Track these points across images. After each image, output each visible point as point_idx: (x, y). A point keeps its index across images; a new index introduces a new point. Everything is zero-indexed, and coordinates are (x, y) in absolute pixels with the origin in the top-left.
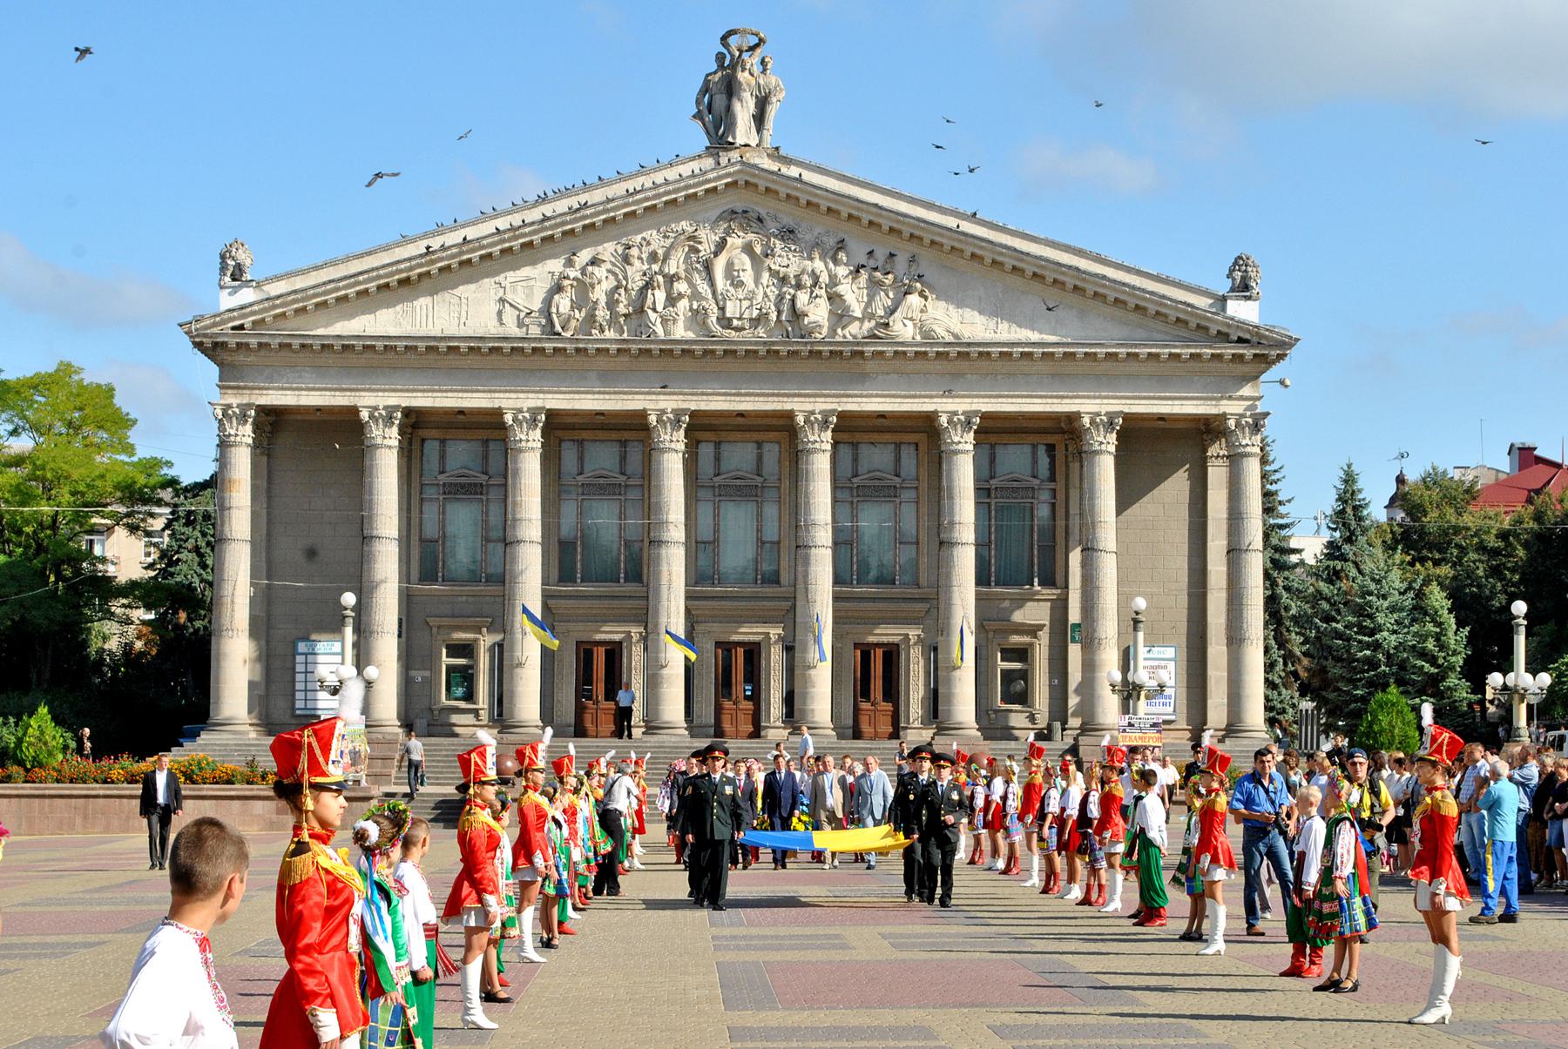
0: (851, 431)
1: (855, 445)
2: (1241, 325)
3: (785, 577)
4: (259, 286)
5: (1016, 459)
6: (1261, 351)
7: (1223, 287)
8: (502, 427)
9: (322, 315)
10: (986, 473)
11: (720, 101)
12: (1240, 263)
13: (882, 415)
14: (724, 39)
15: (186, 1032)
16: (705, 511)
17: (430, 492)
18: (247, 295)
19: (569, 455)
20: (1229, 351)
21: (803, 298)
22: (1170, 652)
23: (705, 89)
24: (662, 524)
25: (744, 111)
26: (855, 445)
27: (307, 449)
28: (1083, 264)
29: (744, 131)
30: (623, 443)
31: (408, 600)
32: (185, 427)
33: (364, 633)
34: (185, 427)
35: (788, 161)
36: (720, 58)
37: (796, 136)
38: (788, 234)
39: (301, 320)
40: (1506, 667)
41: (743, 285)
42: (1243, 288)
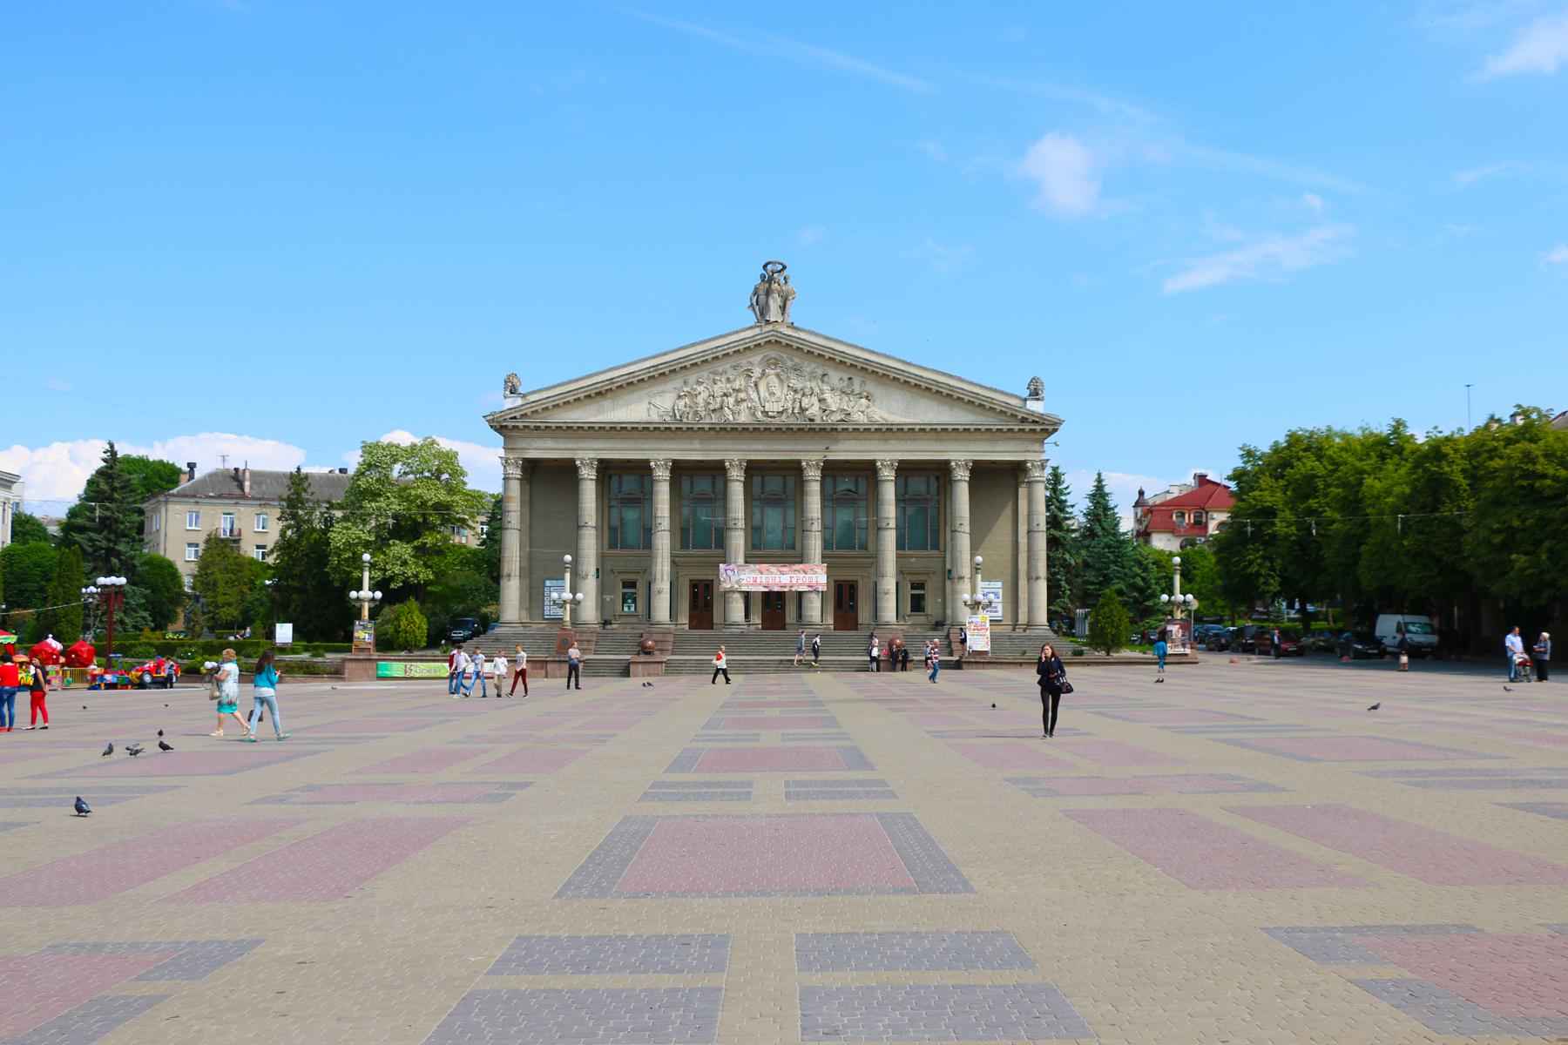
1: (834, 477)
2: (1032, 413)
3: (798, 546)
4: (524, 396)
5: (918, 485)
6: (1044, 428)
7: (1026, 394)
8: (650, 470)
9: (557, 411)
10: (902, 491)
11: (762, 298)
12: (1034, 380)
13: (847, 462)
14: (765, 267)
15: (137, 752)
16: (757, 511)
17: (614, 503)
18: (519, 402)
19: (685, 482)
20: (1027, 427)
21: (805, 401)
22: (999, 584)
23: (756, 293)
24: (732, 515)
25: (774, 304)
26: (834, 477)
27: (546, 480)
28: (952, 382)
29: (774, 314)
30: (714, 477)
31: (602, 558)
32: (486, 467)
33: (576, 576)
34: (486, 467)
35: (797, 329)
36: (763, 277)
37: (811, 315)
38: (796, 369)
39: (545, 414)
40: (359, 589)
41: (772, 396)
42: (1035, 394)
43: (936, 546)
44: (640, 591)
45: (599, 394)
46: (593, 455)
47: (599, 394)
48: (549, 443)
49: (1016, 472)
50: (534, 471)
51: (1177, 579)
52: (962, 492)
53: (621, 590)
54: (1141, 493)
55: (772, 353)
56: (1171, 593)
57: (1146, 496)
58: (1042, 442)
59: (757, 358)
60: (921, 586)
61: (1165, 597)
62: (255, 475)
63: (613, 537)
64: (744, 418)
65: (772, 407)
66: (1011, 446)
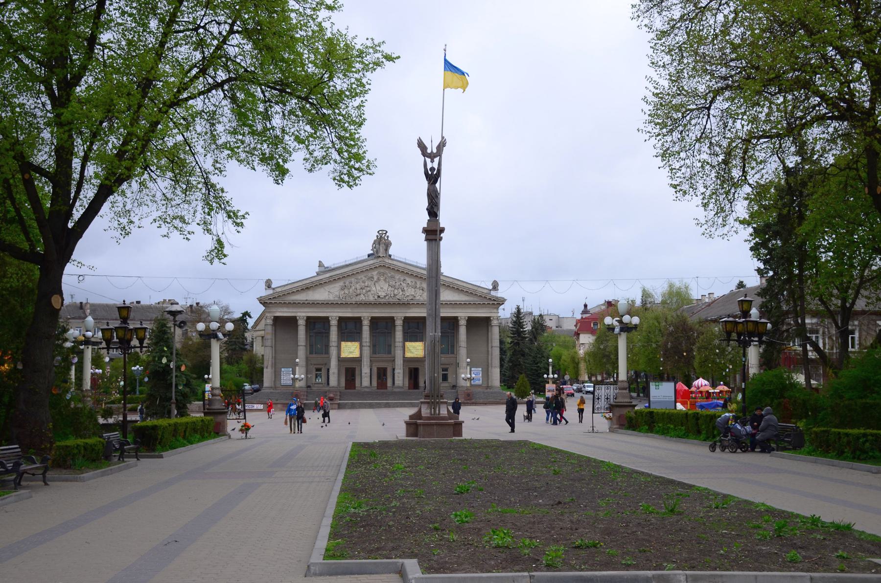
0: (407, 320)
2: (493, 296)
19: (343, 324)
41: (381, 289)
43: (453, 353)
44: (324, 372)
45: (307, 288)
46: (304, 314)
47: (307, 288)
48: (285, 310)
49: (487, 320)
50: (278, 321)
51: (550, 368)
52: (463, 330)
53: (314, 372)
54: (586, 306)
55: (382, 270)
56: (548, 375)
57: (589, 308)
58: (498, 308)
59: (375, 273)
60: (446, 370)
61: (545, 376)
62: (92, 305)
63: (312, 349)
64: (371, 298)
65: (382, 294)
66: (484, 310)
